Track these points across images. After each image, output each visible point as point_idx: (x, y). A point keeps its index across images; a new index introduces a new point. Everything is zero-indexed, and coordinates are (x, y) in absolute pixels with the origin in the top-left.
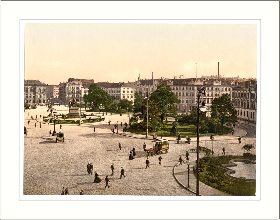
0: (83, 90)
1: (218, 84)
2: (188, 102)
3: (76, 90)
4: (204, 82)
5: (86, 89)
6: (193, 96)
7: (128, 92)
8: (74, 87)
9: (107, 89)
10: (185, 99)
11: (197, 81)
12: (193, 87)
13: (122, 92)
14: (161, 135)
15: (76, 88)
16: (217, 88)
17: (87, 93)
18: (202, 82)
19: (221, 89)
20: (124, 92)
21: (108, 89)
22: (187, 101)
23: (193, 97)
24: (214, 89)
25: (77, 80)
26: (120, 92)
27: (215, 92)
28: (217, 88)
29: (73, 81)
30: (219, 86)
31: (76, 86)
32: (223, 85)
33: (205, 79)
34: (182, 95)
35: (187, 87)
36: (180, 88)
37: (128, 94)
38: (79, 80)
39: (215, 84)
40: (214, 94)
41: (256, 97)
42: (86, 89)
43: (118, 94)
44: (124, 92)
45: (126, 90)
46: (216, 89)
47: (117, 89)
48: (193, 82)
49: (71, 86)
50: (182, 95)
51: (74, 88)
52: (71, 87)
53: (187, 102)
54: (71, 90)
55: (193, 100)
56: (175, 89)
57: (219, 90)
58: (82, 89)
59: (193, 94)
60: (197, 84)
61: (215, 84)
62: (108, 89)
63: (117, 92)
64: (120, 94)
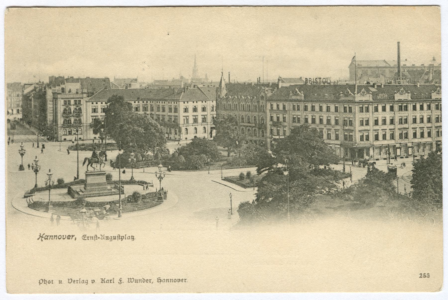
0: (90, 106)
1: (403, 97)
2: (341, 137)
3: (73, 108)
4: (373, 94)
5: (97, 103)
6: (351, 124)
7: (195, 110)
8: (69, 101)
9: (145, 102)
10: (333, 130)
11: (358, 93)
12: (350, 106)
13: (181, 110)
14: (92, 145)
15: (72, 102)
16: (401, 106)
17: (100, 115)
18: (371, 95)
19: (410, 107)
20: (186, 110)
21: (147, 102)
22: (338, 134)
23: (352, 128)
24: (396, 107)
25: (72, 80)
26: (176, 110)
27: (398, 115)
28: (362, 107)
29: (63, 83)
30: (366, 102)
31: (73, 98)
32: (415, 99)
33: (376, 87)
34: (325, 122)
35: (336, 105)
36: (313, 107)
37: (195, 114)
38: (77, 80)
39: (398, 97)
40: (397, 120)
41: (439, 107)
42: (97, 103)
43: (173, 114)
44: (186, 110)
45: (191, 105)
46: (401, 109)
47: (170, 104)
48: (350, 94)
49: (62, 99)
50: (325, 122)
51: (69, 104)
52: (62, 101)
53: (337, 138)
54: (62, 107)
55: (351, 134)
56: (309, 108)
57: (367, 110)
58: (88, 103)
59: (350, 121)
60: (360, 99)
61: (398, 97)
62: (147, 102)
63: (159, 111)
64: (176, 114)
